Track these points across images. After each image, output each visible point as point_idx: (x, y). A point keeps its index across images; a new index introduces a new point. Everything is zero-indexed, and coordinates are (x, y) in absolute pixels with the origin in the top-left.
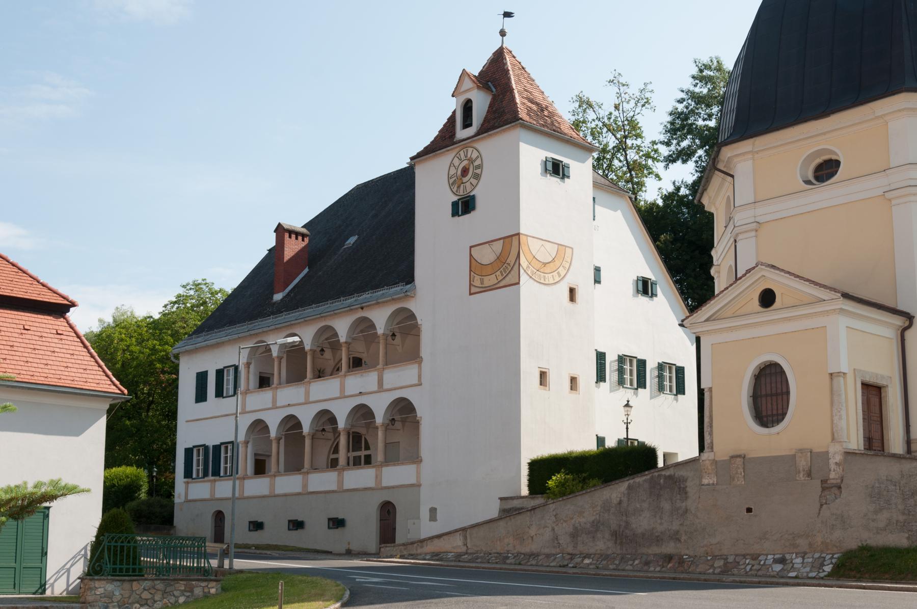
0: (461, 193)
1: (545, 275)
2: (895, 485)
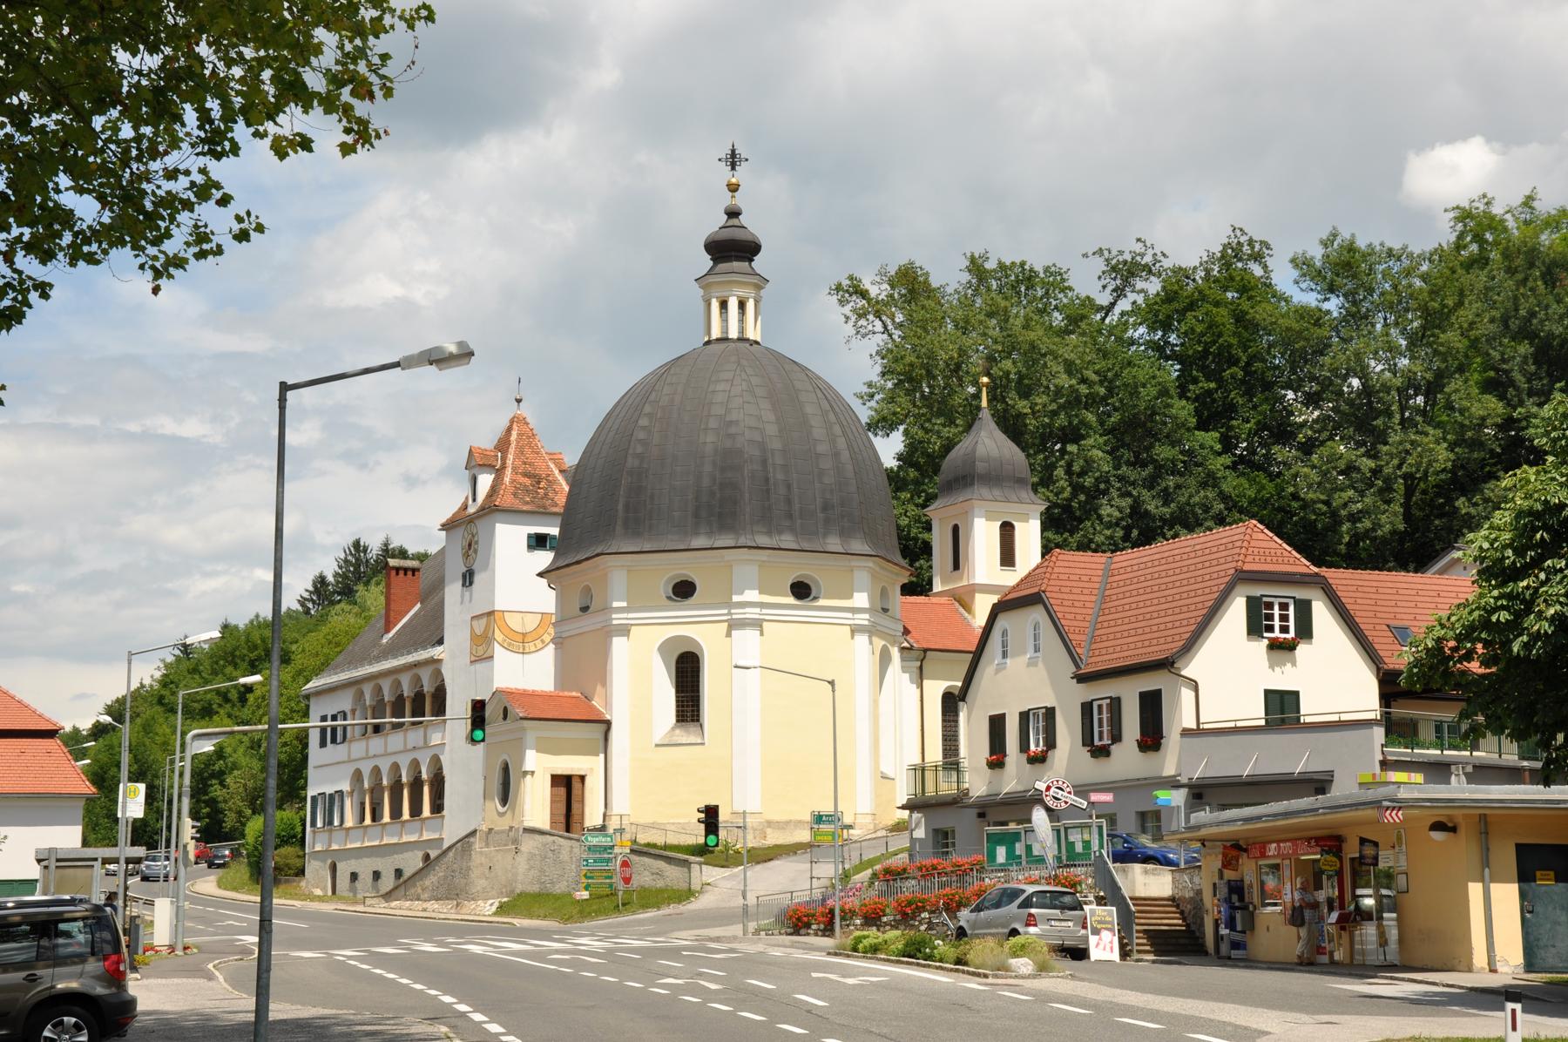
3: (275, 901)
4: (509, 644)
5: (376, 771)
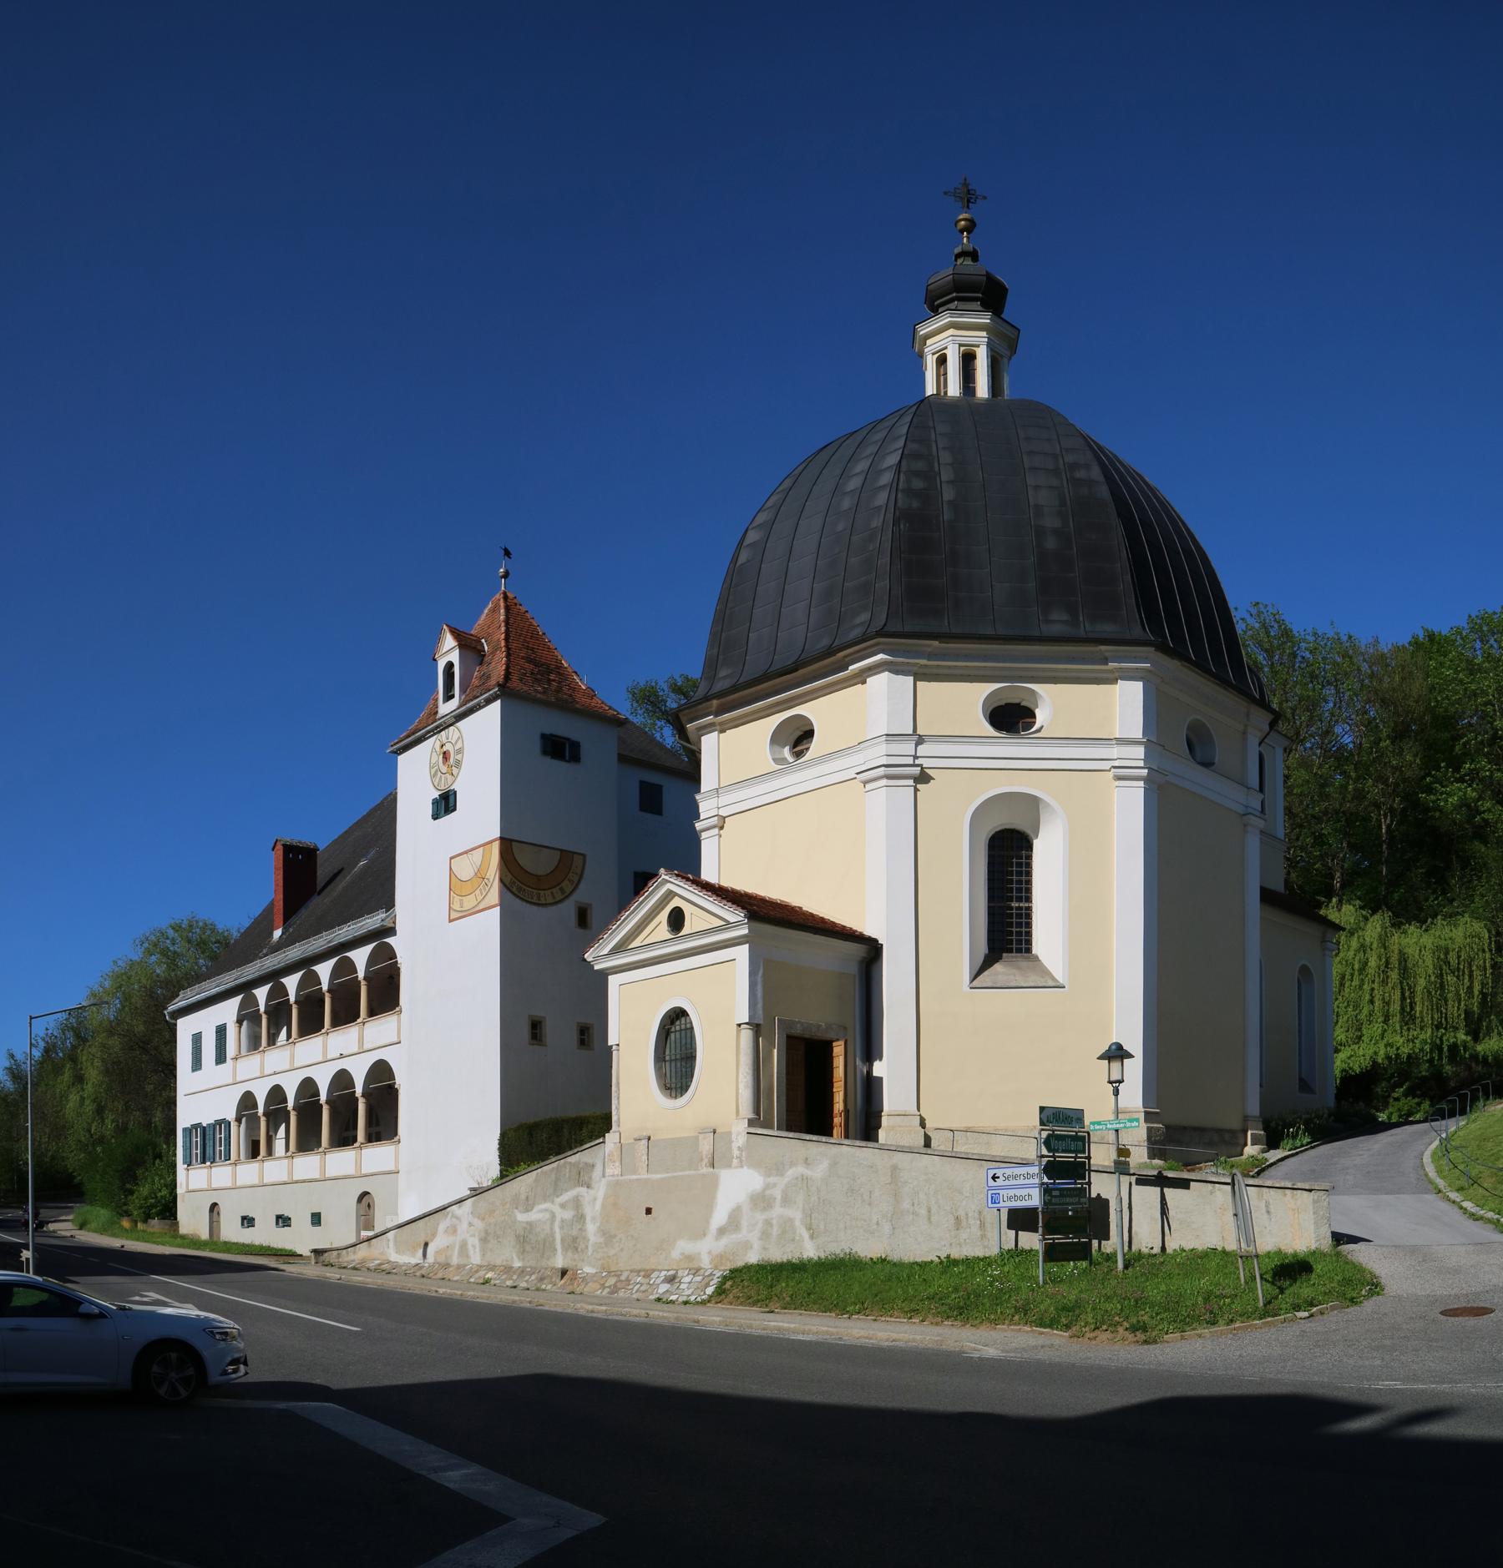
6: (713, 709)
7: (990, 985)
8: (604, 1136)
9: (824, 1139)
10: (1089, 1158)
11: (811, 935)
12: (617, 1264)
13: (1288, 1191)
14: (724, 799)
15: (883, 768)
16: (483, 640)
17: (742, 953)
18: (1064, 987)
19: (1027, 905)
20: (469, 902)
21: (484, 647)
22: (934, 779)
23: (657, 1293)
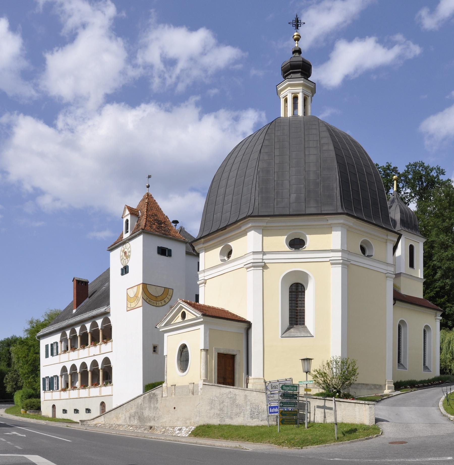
0: (124, 265)
1: (157, 302)
2: (217, 398)
3: (309, 115)
4: (149, 301)
5: (74, 367)
6: (202, 242)
7: (288, 336)
8: (162, 384)
9: (232, 387)
10: (299, 393)
11: (226, 320)
12: (166, 424)
13: (363, 405)
14: (206, 274)
15: (252, 264)
16: (139, 211)
17: (202, 327)
18: (313, 337)
19: (303, 309)
20: (133, 305)
21: (139, 214)
22: (269, 268)
23: (175, 433)
